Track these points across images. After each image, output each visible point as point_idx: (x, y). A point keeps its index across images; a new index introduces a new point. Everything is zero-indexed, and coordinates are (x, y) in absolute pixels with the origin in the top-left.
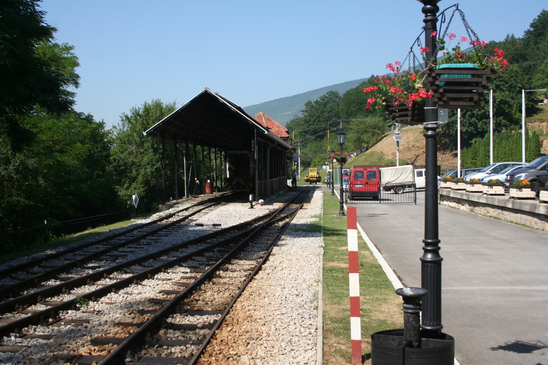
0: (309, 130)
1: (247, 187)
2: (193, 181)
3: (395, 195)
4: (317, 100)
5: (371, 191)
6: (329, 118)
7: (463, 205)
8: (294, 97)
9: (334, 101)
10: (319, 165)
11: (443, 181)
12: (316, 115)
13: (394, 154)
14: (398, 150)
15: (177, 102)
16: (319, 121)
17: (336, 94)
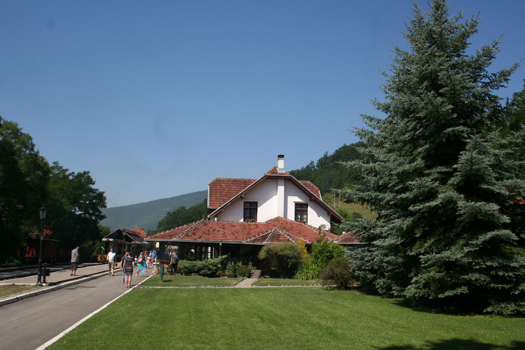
4: (324, 155)
8: (171, 198)
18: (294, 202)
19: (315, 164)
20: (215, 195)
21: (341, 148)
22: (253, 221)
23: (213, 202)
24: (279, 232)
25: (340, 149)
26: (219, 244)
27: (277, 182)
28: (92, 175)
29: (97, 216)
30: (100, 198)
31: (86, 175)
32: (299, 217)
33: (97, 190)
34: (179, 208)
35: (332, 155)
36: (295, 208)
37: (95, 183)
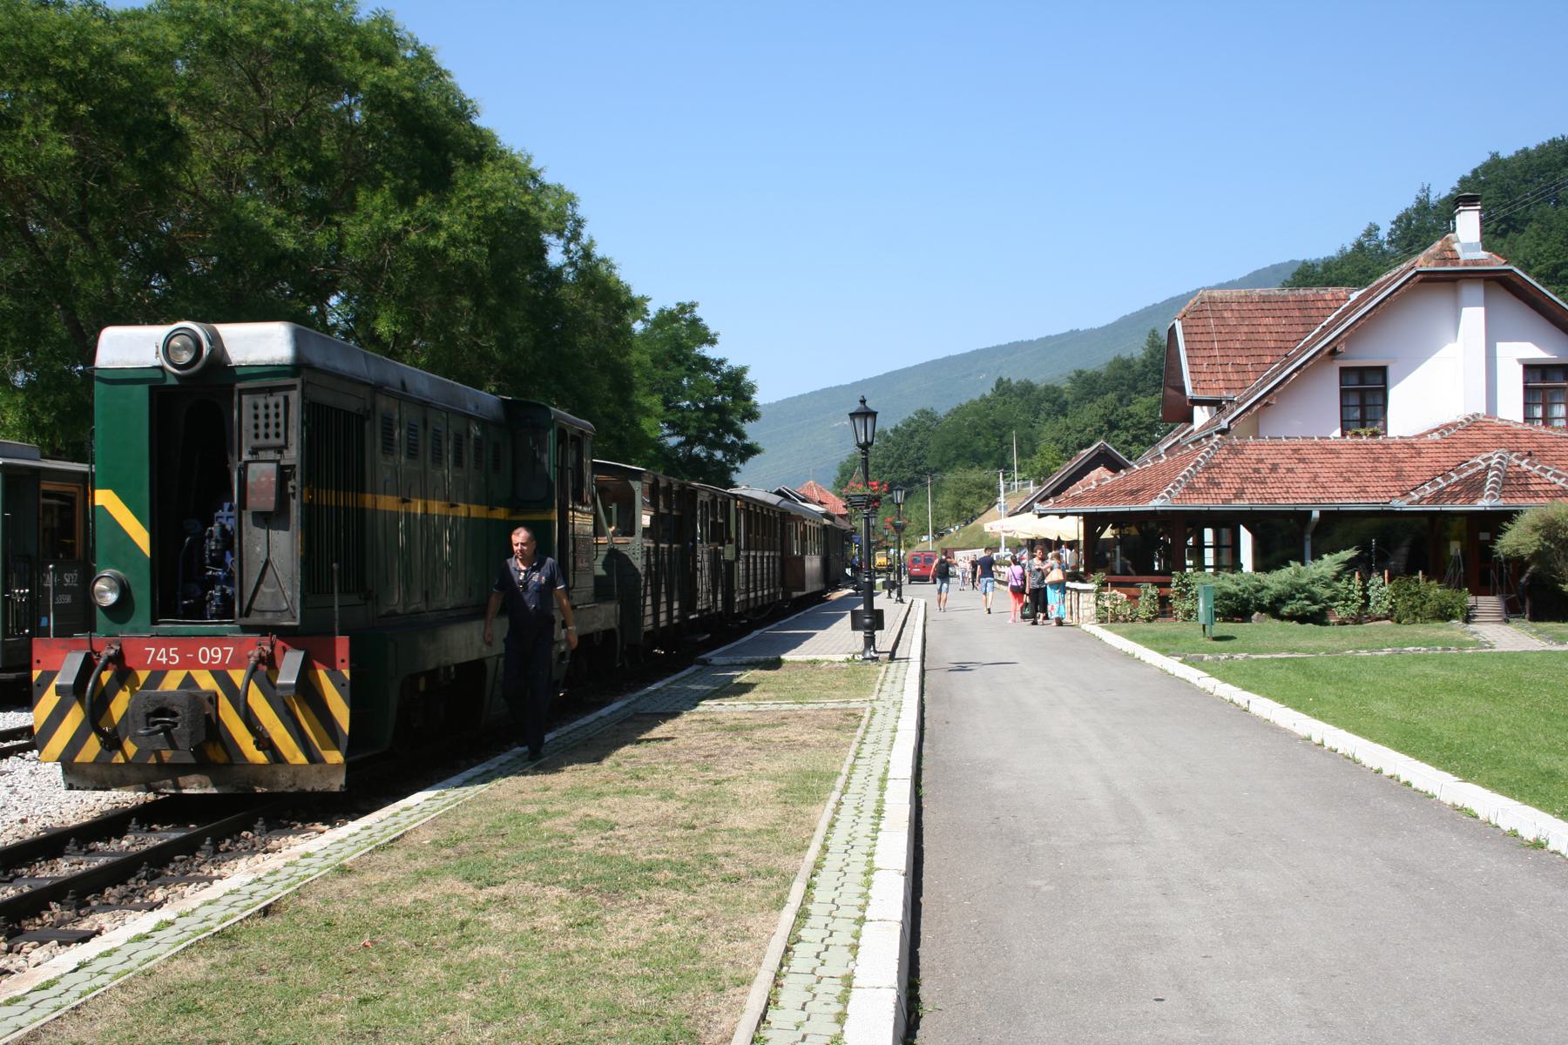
6: (919, 459)
16: (901, 466)
18: (1519, 361)
19: (1383, 234)
20: (1206, 353)
21: (1480, 168)
22: (1375, 434)
23: (1202, 377)
24: (1519, 466)
25: (1475, 172)
26: (1311, 512)
27: (1456, 292)
28: (705, 314)
29: (728, 449)
30: (736, 385)
31: (687, 316)
32: (1538, 412)
33: (721, 362)
35: (1445, 199)
36: (1524, 382)
37: (719, 339)
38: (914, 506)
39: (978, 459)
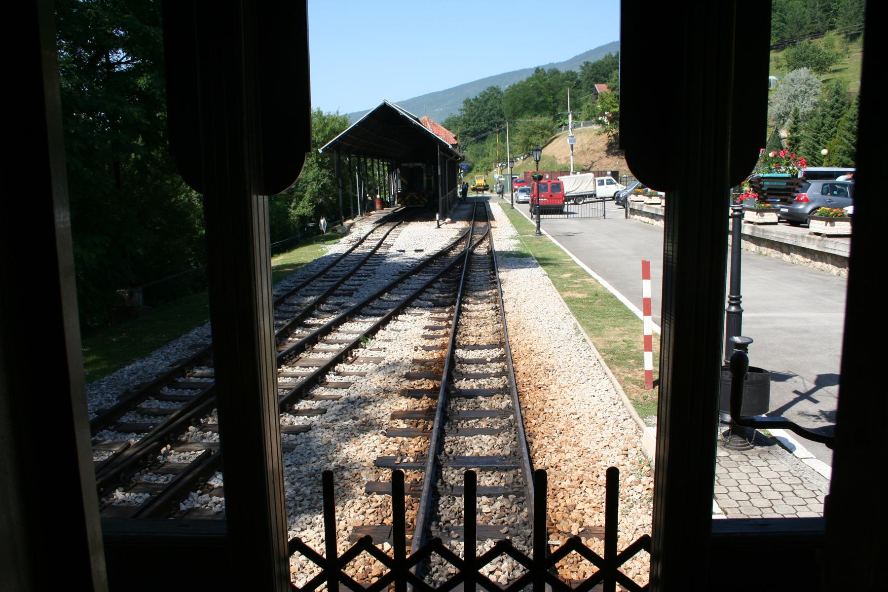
0: (469, 131)
1: (422, 202)
2: (365, 198)
3: (574, 206)
5: (556, 204)
7: (658, 221)
8: (446, 91)
9: (495, 98)
10: (482, 170)
11: (634, 194)
12: (476, 114)
13: (567, 159)
14: (572, 155)
15: (340, 111)
16: (480, 121)
17: (498, 89)
34: (485, 90)
38: (492, 144)
39: (539, 109)
